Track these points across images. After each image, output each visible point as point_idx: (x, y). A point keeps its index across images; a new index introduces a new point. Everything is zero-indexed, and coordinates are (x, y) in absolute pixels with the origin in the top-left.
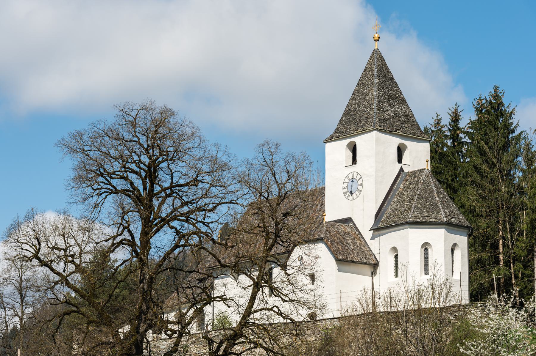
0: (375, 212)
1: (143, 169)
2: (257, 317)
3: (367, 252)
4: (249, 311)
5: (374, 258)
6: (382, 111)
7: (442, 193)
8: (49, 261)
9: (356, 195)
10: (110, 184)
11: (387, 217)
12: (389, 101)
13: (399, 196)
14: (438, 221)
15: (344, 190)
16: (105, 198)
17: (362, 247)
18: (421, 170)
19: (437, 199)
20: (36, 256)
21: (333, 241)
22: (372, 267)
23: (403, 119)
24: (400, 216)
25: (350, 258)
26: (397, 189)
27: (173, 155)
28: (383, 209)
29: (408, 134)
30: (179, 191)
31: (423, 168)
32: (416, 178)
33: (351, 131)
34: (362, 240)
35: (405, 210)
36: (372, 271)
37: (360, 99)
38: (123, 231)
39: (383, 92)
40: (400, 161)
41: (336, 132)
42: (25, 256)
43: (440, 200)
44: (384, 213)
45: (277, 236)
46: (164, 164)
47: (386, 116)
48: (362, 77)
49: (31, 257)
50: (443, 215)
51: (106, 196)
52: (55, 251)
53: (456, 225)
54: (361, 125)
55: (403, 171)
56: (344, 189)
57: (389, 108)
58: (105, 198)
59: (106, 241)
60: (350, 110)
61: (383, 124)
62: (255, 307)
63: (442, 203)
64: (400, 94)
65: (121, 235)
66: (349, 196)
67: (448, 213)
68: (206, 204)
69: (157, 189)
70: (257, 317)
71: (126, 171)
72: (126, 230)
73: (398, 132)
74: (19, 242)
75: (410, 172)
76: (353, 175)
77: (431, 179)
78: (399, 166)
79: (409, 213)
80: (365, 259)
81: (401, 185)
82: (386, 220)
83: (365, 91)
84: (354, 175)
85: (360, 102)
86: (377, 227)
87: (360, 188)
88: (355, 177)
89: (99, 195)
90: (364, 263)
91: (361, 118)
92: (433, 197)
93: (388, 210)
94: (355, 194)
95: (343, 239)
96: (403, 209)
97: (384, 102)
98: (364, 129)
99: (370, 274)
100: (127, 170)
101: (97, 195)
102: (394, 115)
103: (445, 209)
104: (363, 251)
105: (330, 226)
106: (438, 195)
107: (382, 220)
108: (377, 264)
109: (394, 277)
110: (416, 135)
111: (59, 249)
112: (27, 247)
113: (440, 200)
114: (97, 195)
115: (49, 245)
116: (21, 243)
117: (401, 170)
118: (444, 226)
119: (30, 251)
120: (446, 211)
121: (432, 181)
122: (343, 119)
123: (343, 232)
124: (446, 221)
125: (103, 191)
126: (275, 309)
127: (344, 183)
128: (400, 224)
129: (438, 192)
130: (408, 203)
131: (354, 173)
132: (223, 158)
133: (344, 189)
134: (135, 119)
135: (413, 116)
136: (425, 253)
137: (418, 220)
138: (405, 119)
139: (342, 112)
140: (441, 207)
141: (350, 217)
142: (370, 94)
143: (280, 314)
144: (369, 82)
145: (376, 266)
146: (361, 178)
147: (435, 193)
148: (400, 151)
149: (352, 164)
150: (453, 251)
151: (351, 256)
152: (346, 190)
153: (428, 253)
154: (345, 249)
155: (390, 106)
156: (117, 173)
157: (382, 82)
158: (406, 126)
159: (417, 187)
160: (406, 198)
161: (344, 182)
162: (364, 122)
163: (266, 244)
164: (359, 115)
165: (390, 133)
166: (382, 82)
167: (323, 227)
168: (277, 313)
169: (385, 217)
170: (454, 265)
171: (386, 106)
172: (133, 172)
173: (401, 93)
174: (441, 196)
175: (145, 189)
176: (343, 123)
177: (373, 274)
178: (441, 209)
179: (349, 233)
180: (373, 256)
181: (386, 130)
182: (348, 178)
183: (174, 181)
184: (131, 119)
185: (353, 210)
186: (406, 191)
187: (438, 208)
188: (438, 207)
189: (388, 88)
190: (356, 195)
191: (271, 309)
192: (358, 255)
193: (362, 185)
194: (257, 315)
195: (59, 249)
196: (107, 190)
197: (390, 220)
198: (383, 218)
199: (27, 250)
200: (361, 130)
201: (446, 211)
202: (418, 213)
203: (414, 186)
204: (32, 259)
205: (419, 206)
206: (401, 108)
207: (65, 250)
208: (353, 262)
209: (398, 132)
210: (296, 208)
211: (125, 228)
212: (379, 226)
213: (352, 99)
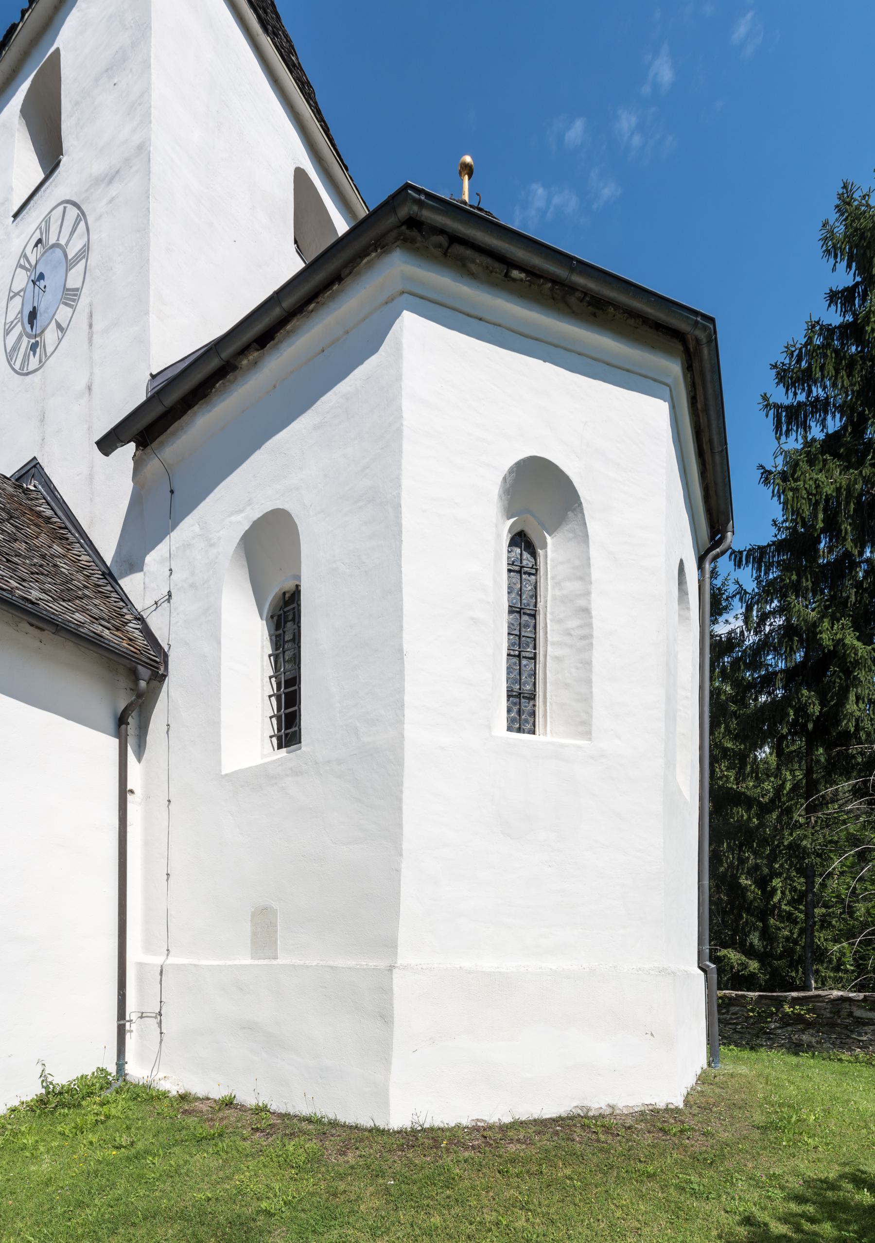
36: (122, 706)
141: (107, 454)
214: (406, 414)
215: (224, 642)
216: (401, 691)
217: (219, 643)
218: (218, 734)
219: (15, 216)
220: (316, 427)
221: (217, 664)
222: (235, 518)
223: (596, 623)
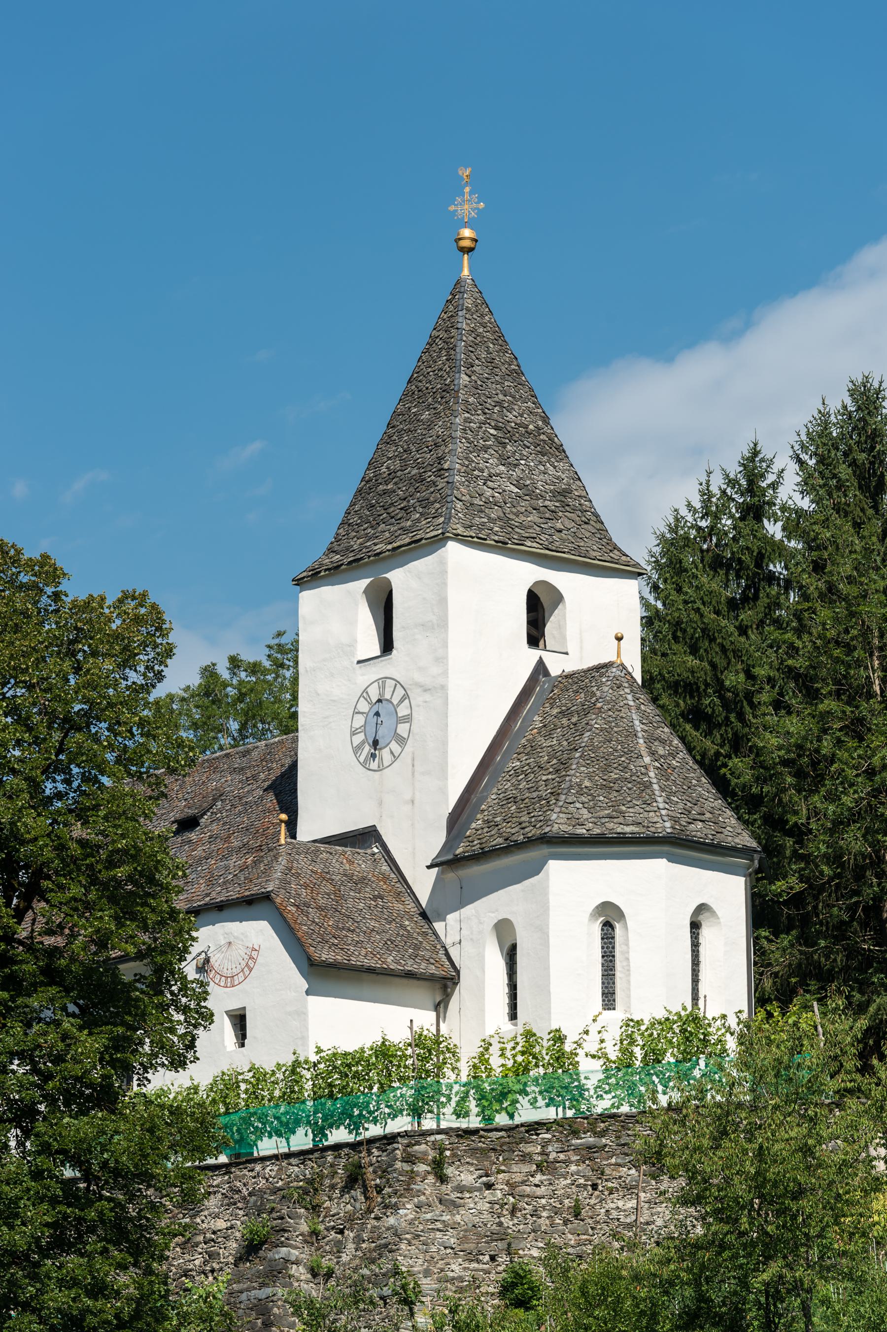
3: (420, 939)
5: (444, 959)
6: (477, 477)
7: (663, 742)
9: (392, 753)
11: (484, 821)
12: (504, 445)
13: (527, 754)
14: (643, 830)
15: (354, 738)
17: (407, 923)
19: (647, 760)
21: (305, 904)
22: (438, 986)
23: (547, 503)
24: (523, 819)
25: (360, 958)
29: (564, 552)
31: (607, 661)
32: (582, 695)
33: (375, 544)
34: (408, 900)
36: (438, 1000)
39: (482, 418)
40: (535, 638)
41: (331, 550)
43: (657, 764)
44: (477, 810)
47: (489, 493)
50: (664, 812)
53: (704, 844)
54: (409, 523)
55: (546, 673)
56: (353, 733)
57: (502, 468)
61: (477, 520)
63: (664, 773)
64: (540, 423)
73: (529, 544)
75: (566, 677)
76: (382, 688)
77: (630, 697)
79: (551, 808)
80: (410, 962)
81: (536, 718)
82: (479, 832)
83: (426, 416)
84: (384, 688)
86: (450, 857)
87: (403, 729)
88: (387, 696)
90: (410, 975)
91: (409, 501)
92: (633, 755)
93: (489, 800)
94: (387, 749)
95: (339, 897)
96: (535, 795)
97: (486, 449)
98: (415, 538)
99: (432, 1007)
102: (516, 490)
104: (409, 935)
105: (299, 854)
106: (649, 748)
107: (468, 833)
108: (452, 979)
109: (507, 1018)
113: (657, 764)
117: (541, 668)
118: (666, 848)
120: (675, 799)
121: (631, 703)
122: (357, 508)
123: (345, 875)
124: (669, 830)
127: (356, 715)
128: (523, 843)
129: (651, 739)
130: (550, 777)
131: (384, 683)
133: (353, 733)
136: (602, 939)
137: (581, 831)
138: (557, 504)
139: (355, 484)
140: (656, 787)
141: (374, 826)
142: (440, 423)
144: (439, 386)
145: (449, 984)
146: (406, 697)
147: (641, 741)
149: (378, 652)
150: (695, 926)
151: (363, 952)
153: (613, 938)
154: (343, 928)
155: (503, 460)
157: (479, 383)
158: (559, 525)
160: (546, 758)
162: (418, 515)
165: (501, 547)
166: (479, 383)
167: (276, 857)
169: (480, 822)
171: (491, 461)
174: (661, 751)
178: (657, 793)
179: (364, 878)
180: (442, 952)
181: (485, 539)
182: (368, 699)
185: (381, 803)
187: (648, 791)
188: (648, 785)
190: (392, 753)
192: (388, 949)
193: (408, 719)
197: (493, 833)
198: (474, 825)
200: (407, 540)
201: (675, 799)
202: (580, 806)
203: (574, 720)
206: (542, 468)
208: (371, 970)
209: (529, 544)
210: (219, 803)
212: (458, 852)
213: (387, 440)
214: (551, 901)
215: (486, 970)
216: (550, 1007)
217: (484, 971)
218: (484, 1016)
219: (359, 662)
220: (523, 891)
221: (483, 982)
222: (492, 915)
223: (632, 964)
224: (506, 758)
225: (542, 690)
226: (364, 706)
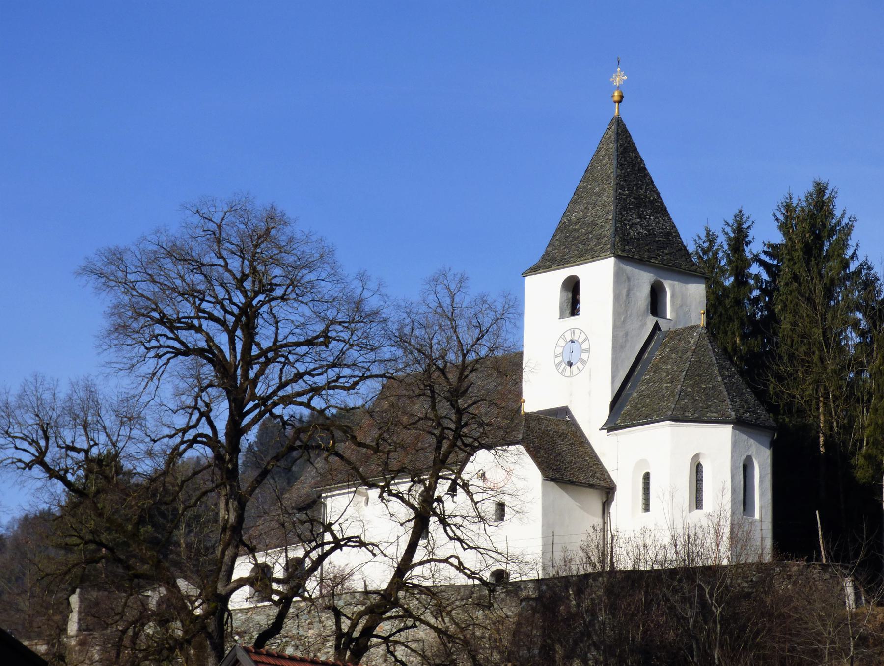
0: (609, 400)
1: (232, 313)
2: (419, 575)
4: (405, 565)
8: (63, 469)
10: (177, 339)
16: (166, 364)
18: (691, 328)
20: (40, 460)
26: (649, 360)
27: (286, 291)
28: (624, 393)
30: (290, 353)
33: (571, 258)
35: (663, 396)
37: (588, 203)
38: (199, 420)
42: (20, 461)
45: (458, 436)
46: (265, 308)
48: (591, 165)
49: (31, 462)
51: (169, 360)
52: (69, 452)
55: (660, 330)
56: (556, 357)
57: (638, 220)
58: (166, 364)
59: (171, 437)
60: (569, 221)
62: (416, 559)
65: (195, 426)
66: (564, 370)
67: (738, 403)
68: (339, 378)
69: (255, 351)
70: (419, 575)
71: (199, 318)
72: (204, 418)
74: (10, 436)
76: (573, 333)
78: (651, 321)
80: (591, 479)
85: (587, 208)
87: (584, 356)
88: (576, 338)
89: (158, 357)
90: (591, 486)
97: (630, 209)
100: (201, 314)
101: (155, 357)
103: (734, 397)
106: (720, 373)
110: (683, 267)
111: (78, 451)
112: (25, 445)
114: (155, 357)
115: (60, 442)
116: (14, 437)
117: (656, 327)
119: (29, 452)
125: (165, 350)
126: (453, 561)
132: (372, 303)
133: (556, 357)
134: (219, 226)
135: (678, 235)
143: (461, 568)
146: (586, 339)
148: (656, 296)
152: (560, 359)
156: (183, 320)
159: (685, 357)
160: (665, 374)
161: (557, 346)
163: (438, 448)
164: (586, 230)
168: (458, 568)
170: (747, 494)
172: (211, 317)
173: (658, 194)
175: (233, 349)
176: (557, 243)
177: (606, 505)
179: (564, 434)
183: (280, 338)
184: (213, 227)
186: (665, 363)
189: (635, 185)
191: (446, 561)
193: (587, 351)
194: (417, 571)
195: (78, 451)
196: (171, 350)
199: (24, 450)
204: (33, 464)
205: (689, 390)
207: (87, 452)
211: (202, 415)
213: (574, 202)
224: (641, 374)
225: (658, 339)
226: (562, 343)
